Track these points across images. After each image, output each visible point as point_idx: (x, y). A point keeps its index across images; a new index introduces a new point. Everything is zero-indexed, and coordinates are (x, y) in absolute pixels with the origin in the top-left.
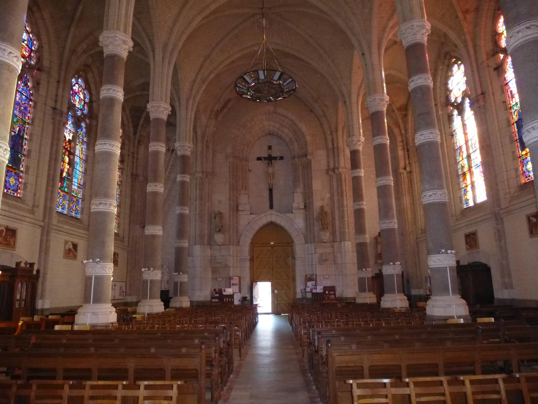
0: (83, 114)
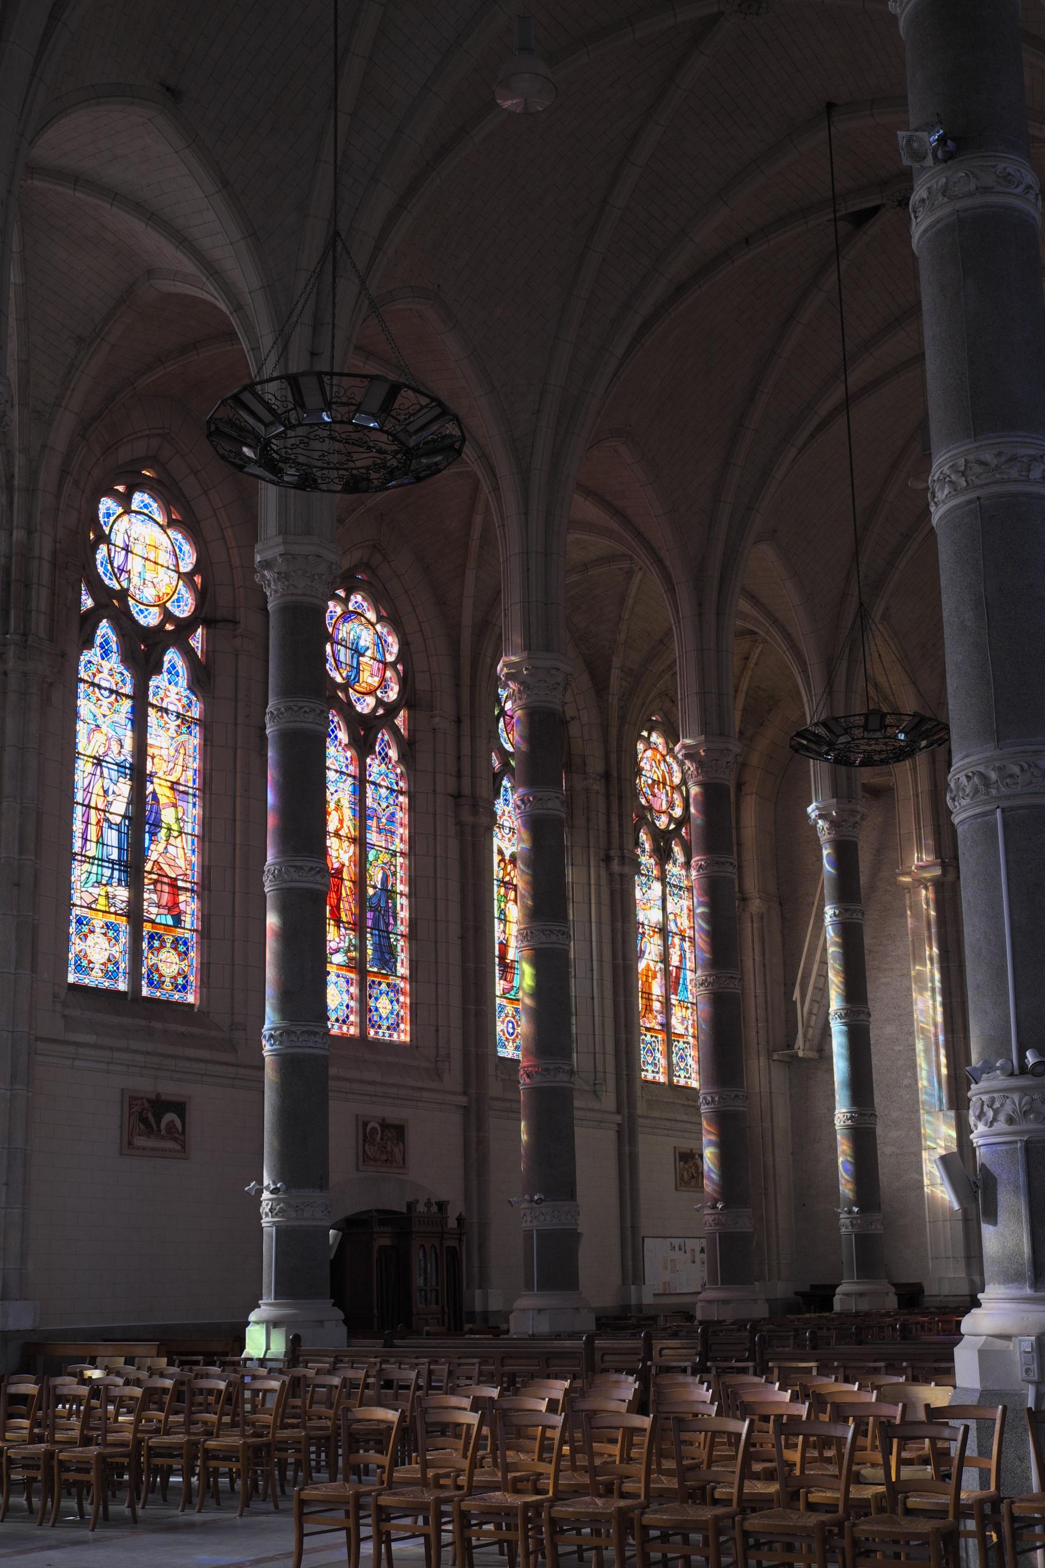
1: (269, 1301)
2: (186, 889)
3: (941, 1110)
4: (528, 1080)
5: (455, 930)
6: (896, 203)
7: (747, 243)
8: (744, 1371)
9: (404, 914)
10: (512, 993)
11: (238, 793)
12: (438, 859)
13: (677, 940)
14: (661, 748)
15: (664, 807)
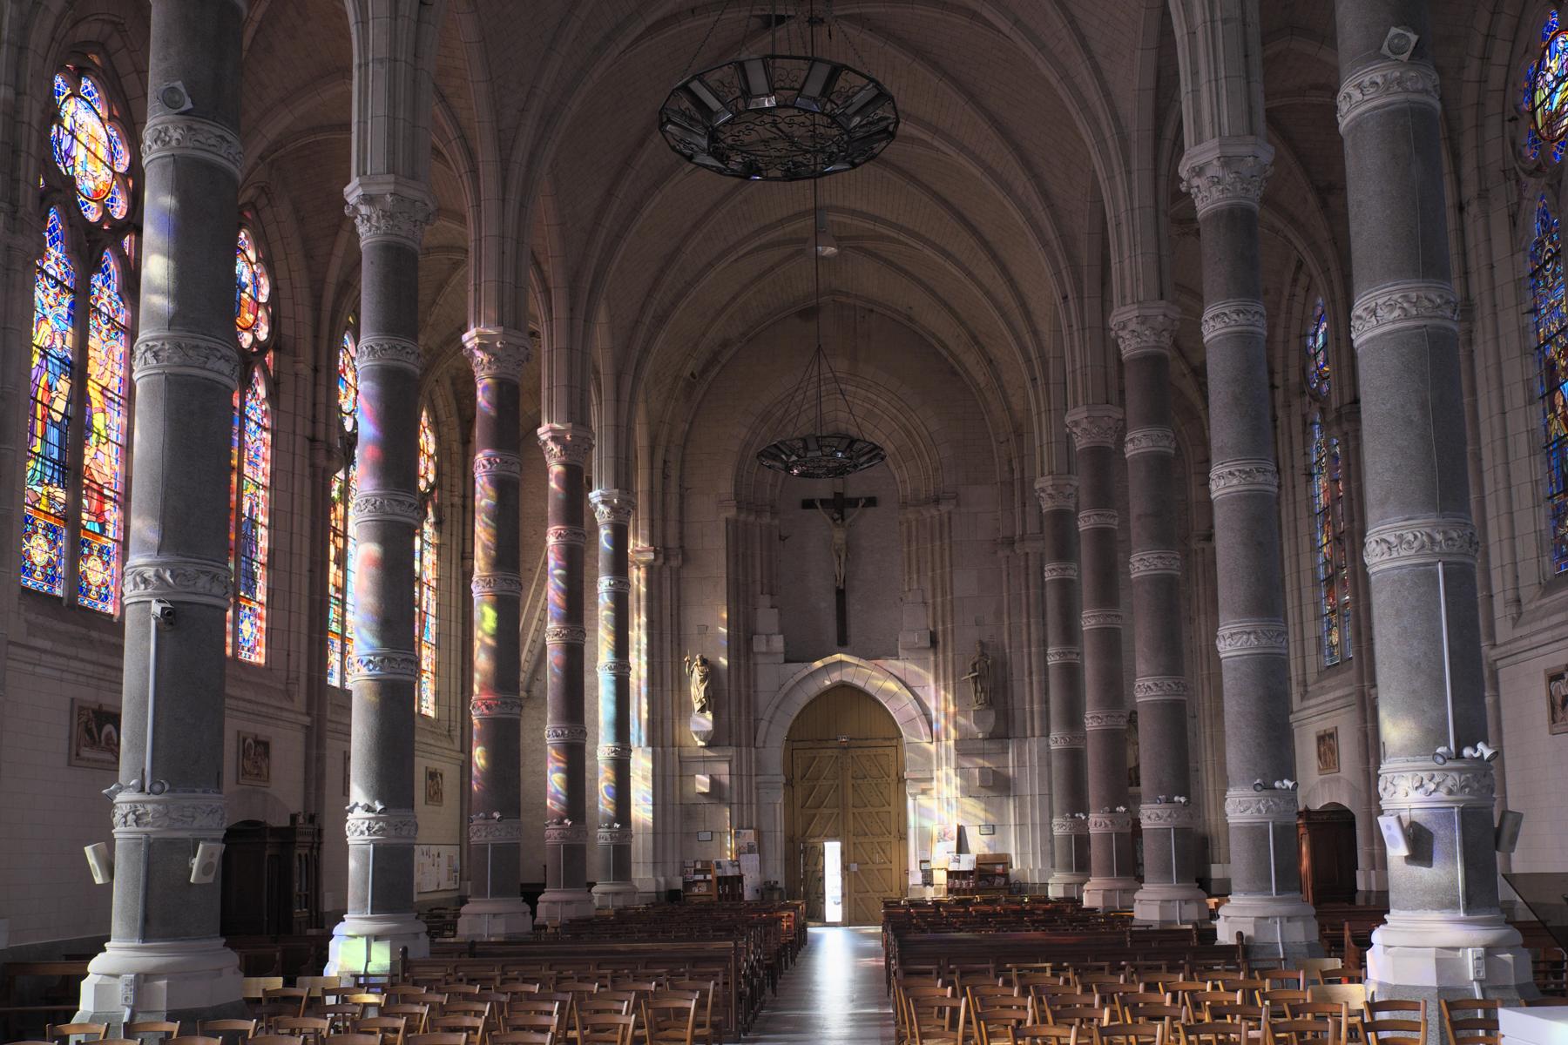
0: (107, 215)
2: (110, 498)
8: (1340, 982)
9: (263, 544)
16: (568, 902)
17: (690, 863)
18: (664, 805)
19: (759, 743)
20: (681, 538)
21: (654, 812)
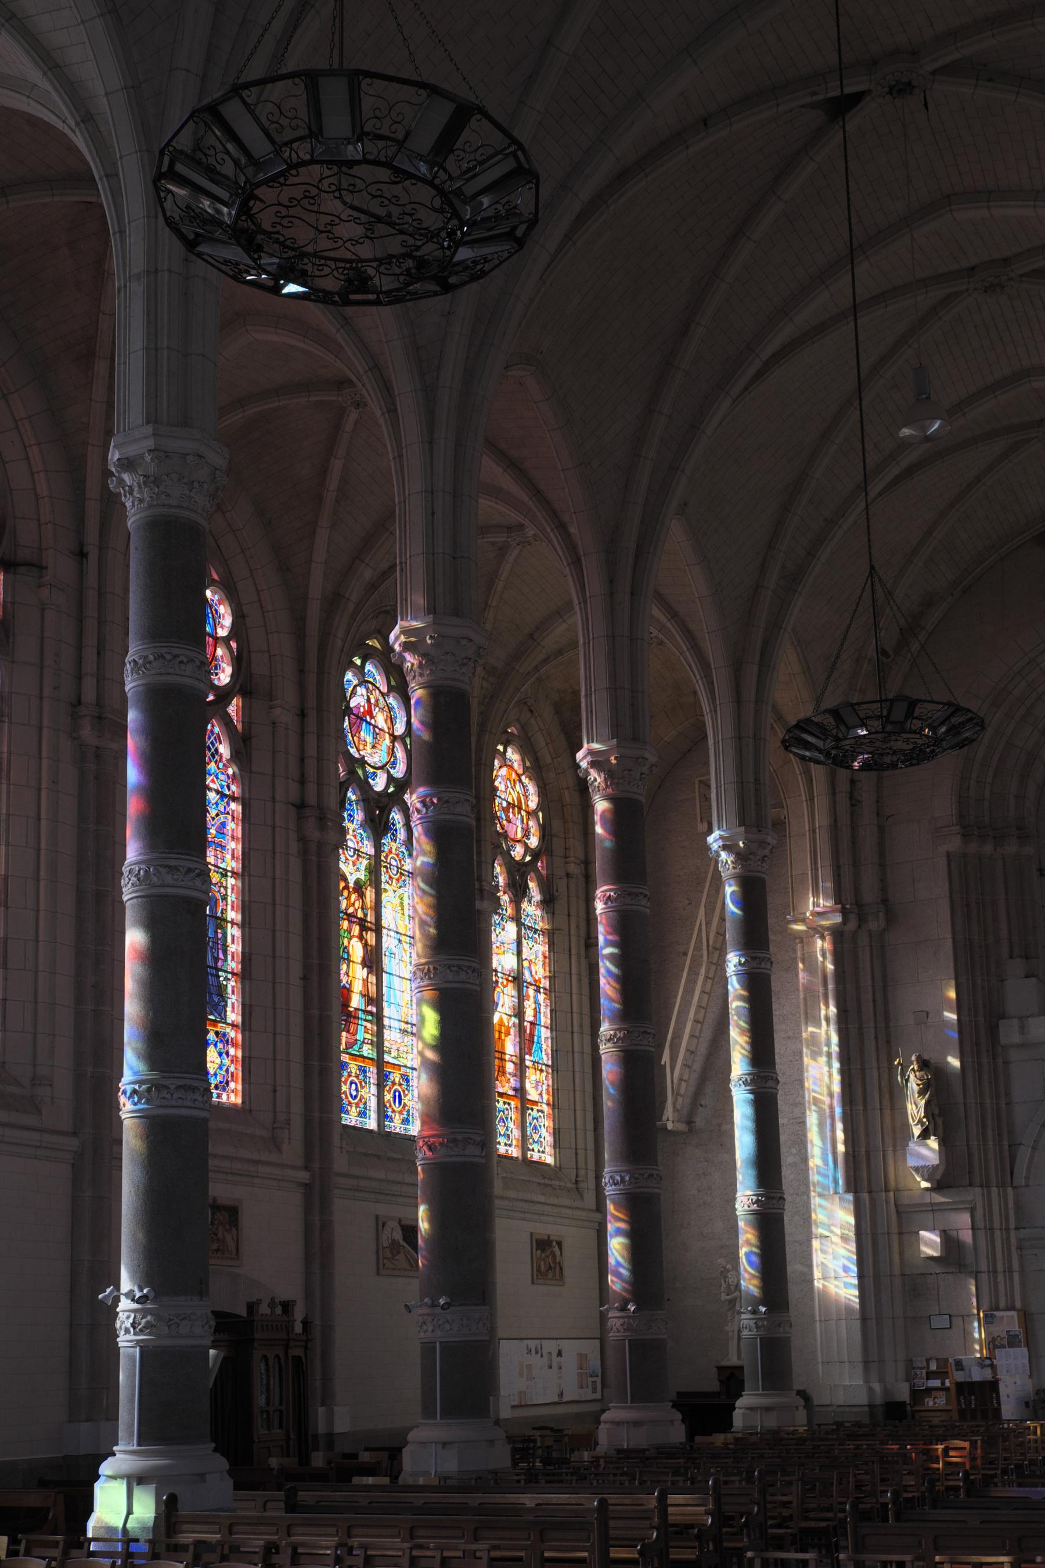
1: (130, 1448)
3: (836, 1193)
4: (429, 1154)
5: (296, 970)
6: (886, 90)
7: (705, 125)
9: (235, 948)
10: (356, 1047)
11: (44, 786)
12: (278, 882)
13: (531, 992)
14: (516, 766)
15: (519, 836)
16: (637, 1424)
17: (920, 1362)
18: (877, 1276)
19: (1020, 1179)
20: (884, 889)
21: (862, 1287)
